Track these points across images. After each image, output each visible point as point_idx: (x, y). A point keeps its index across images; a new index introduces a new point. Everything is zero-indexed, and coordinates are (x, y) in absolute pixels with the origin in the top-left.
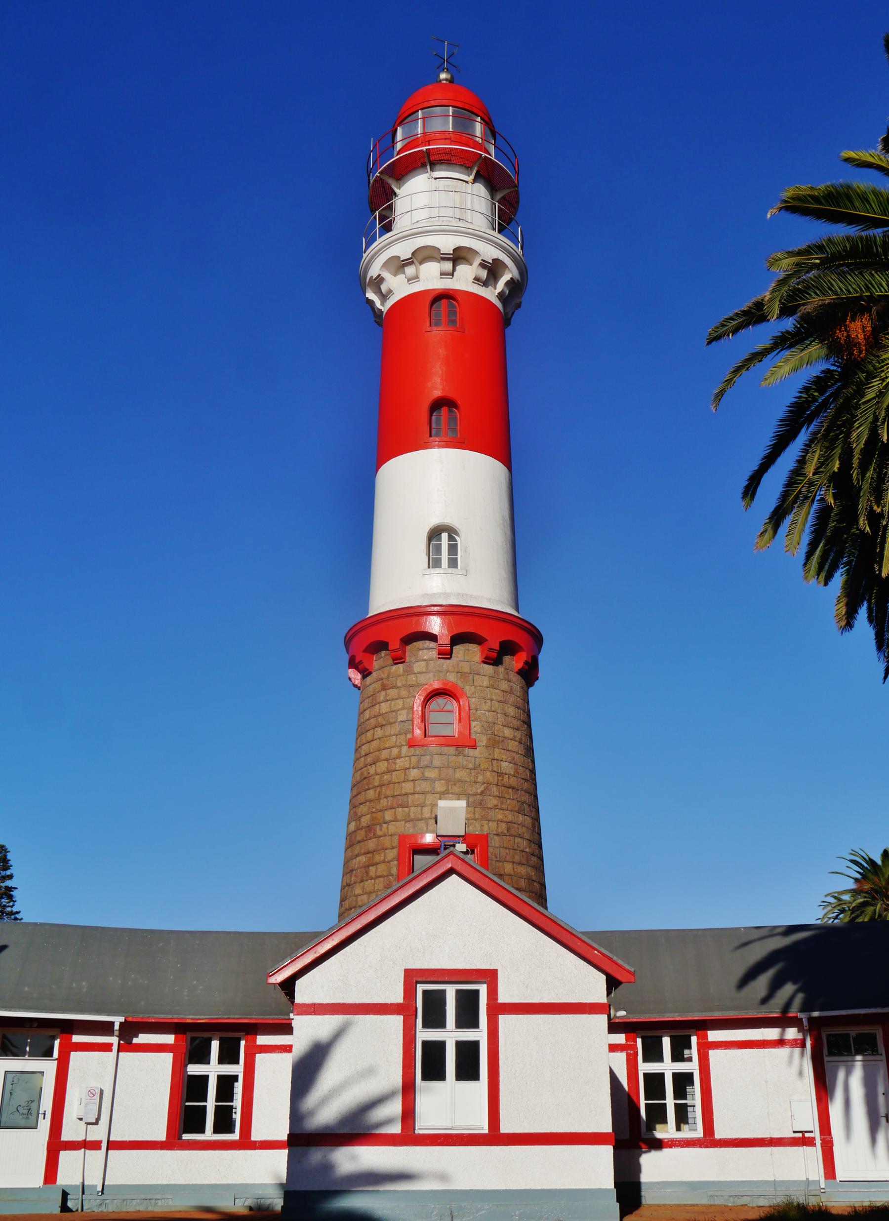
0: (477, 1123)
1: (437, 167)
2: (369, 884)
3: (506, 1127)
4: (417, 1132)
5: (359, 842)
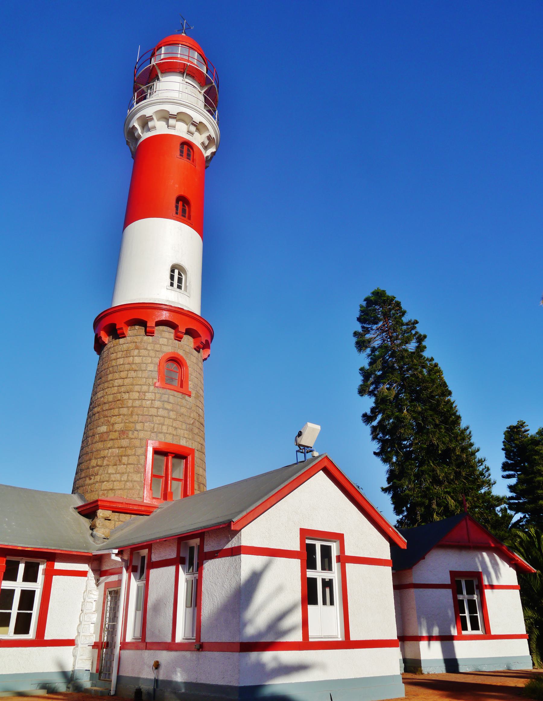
0: (334, 634)
1: (188, 77)
2: (121, 468)
3: (353, 638)
4: (310, 640)
5: (112, 440)
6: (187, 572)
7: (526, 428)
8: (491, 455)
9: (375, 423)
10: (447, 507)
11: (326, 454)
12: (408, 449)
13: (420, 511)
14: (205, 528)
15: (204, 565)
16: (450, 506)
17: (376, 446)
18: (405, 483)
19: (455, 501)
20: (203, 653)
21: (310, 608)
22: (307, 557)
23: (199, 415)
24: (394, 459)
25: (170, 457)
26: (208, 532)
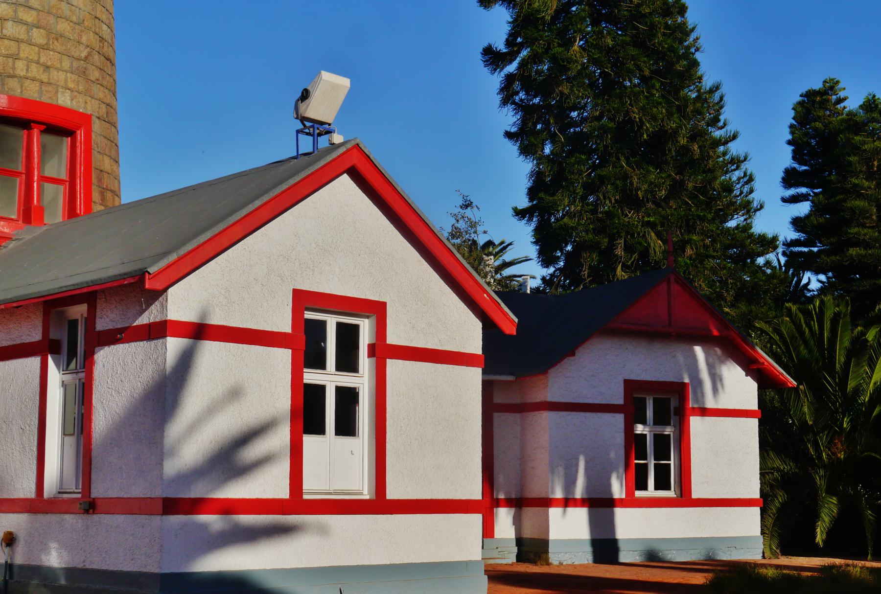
3: (392, 493)
6: (65, 368)
7: (842, 94)
8: (761, 149)
9: (512, 68)
10: (645, 253)
11: (358, 141)
12: (578, 129)
13: (591, 259)
14: (94, 283)
15: (96, 357)
16: (652, 251)
17: (509, 119)
18: (561, 200)
19: (664, 242)
20: (96, 517)
21: (309, 441)
22: (307, 347)
23: (102, 39)
24: (547, 150)
25: (36, 132)
26: (103, 291)
